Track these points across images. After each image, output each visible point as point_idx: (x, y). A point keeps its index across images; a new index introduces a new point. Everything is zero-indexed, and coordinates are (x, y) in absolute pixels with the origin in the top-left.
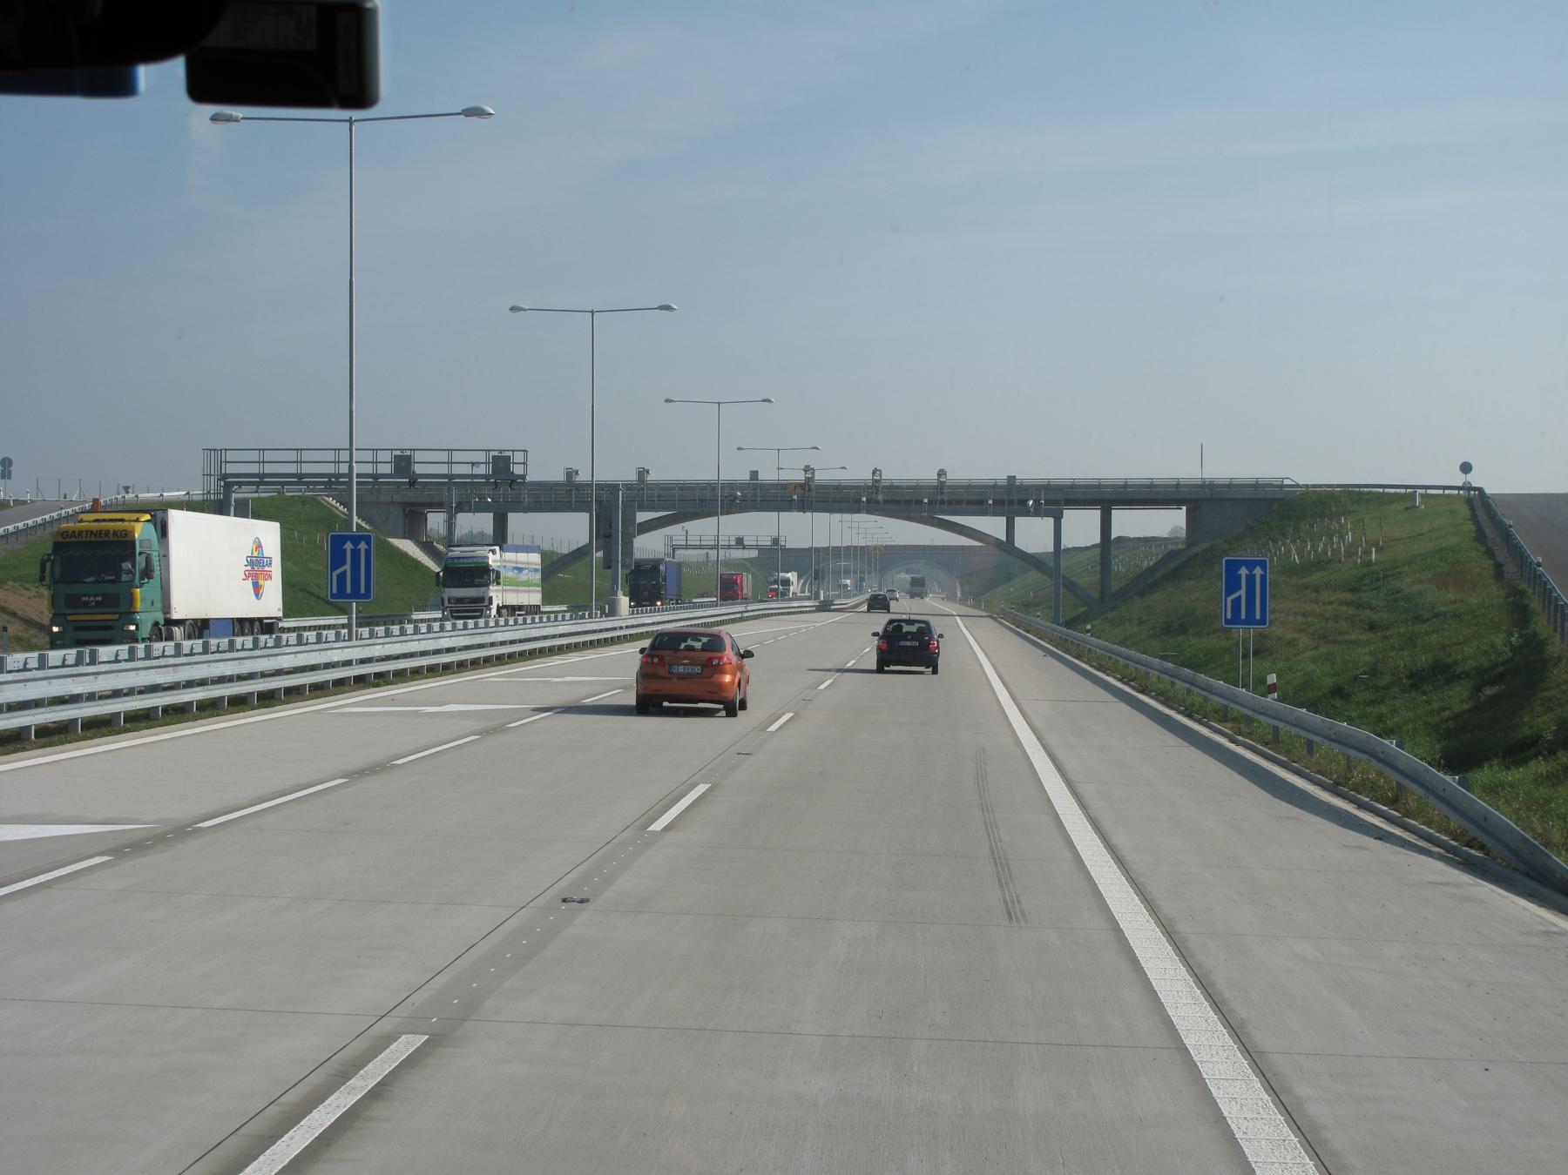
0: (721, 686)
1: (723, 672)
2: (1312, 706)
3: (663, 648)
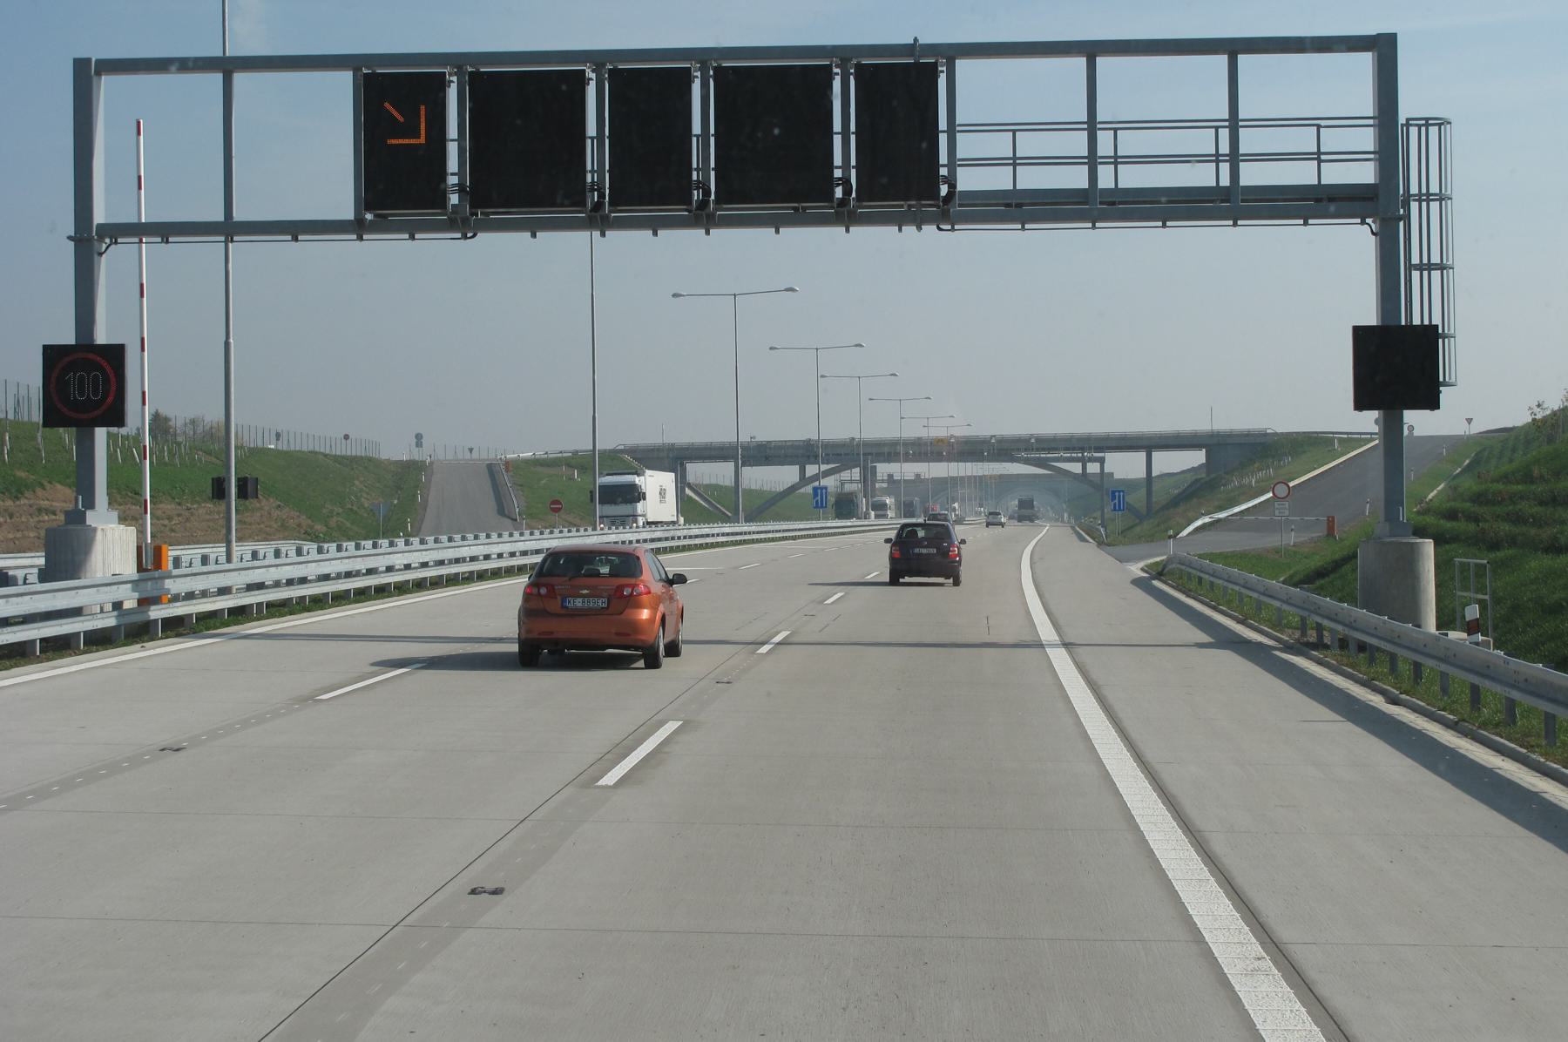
0: (635, 626)
1: (640, 606)
2: (1295, 585)
3: (555, 578)
